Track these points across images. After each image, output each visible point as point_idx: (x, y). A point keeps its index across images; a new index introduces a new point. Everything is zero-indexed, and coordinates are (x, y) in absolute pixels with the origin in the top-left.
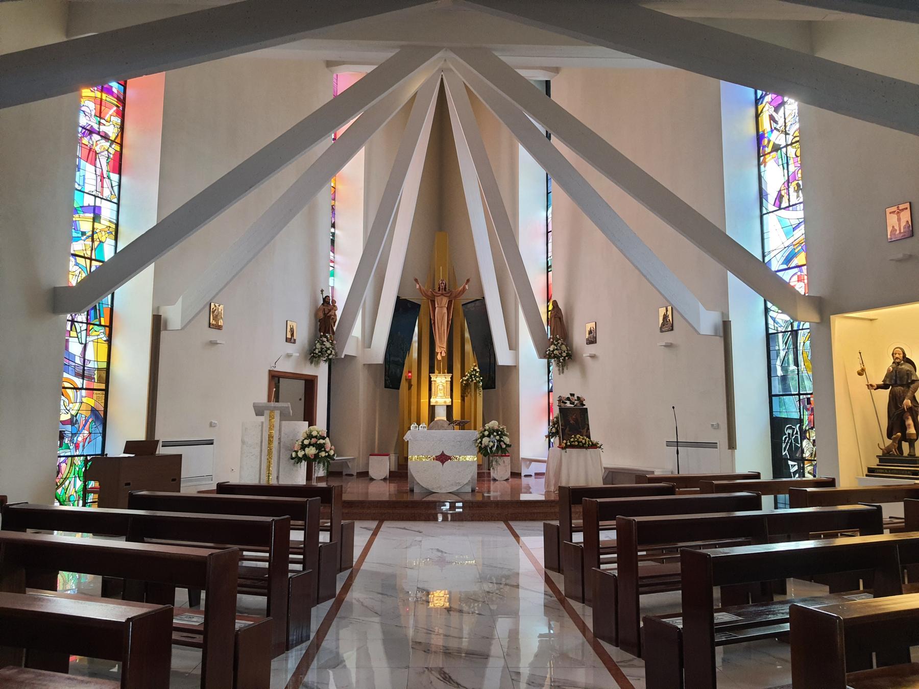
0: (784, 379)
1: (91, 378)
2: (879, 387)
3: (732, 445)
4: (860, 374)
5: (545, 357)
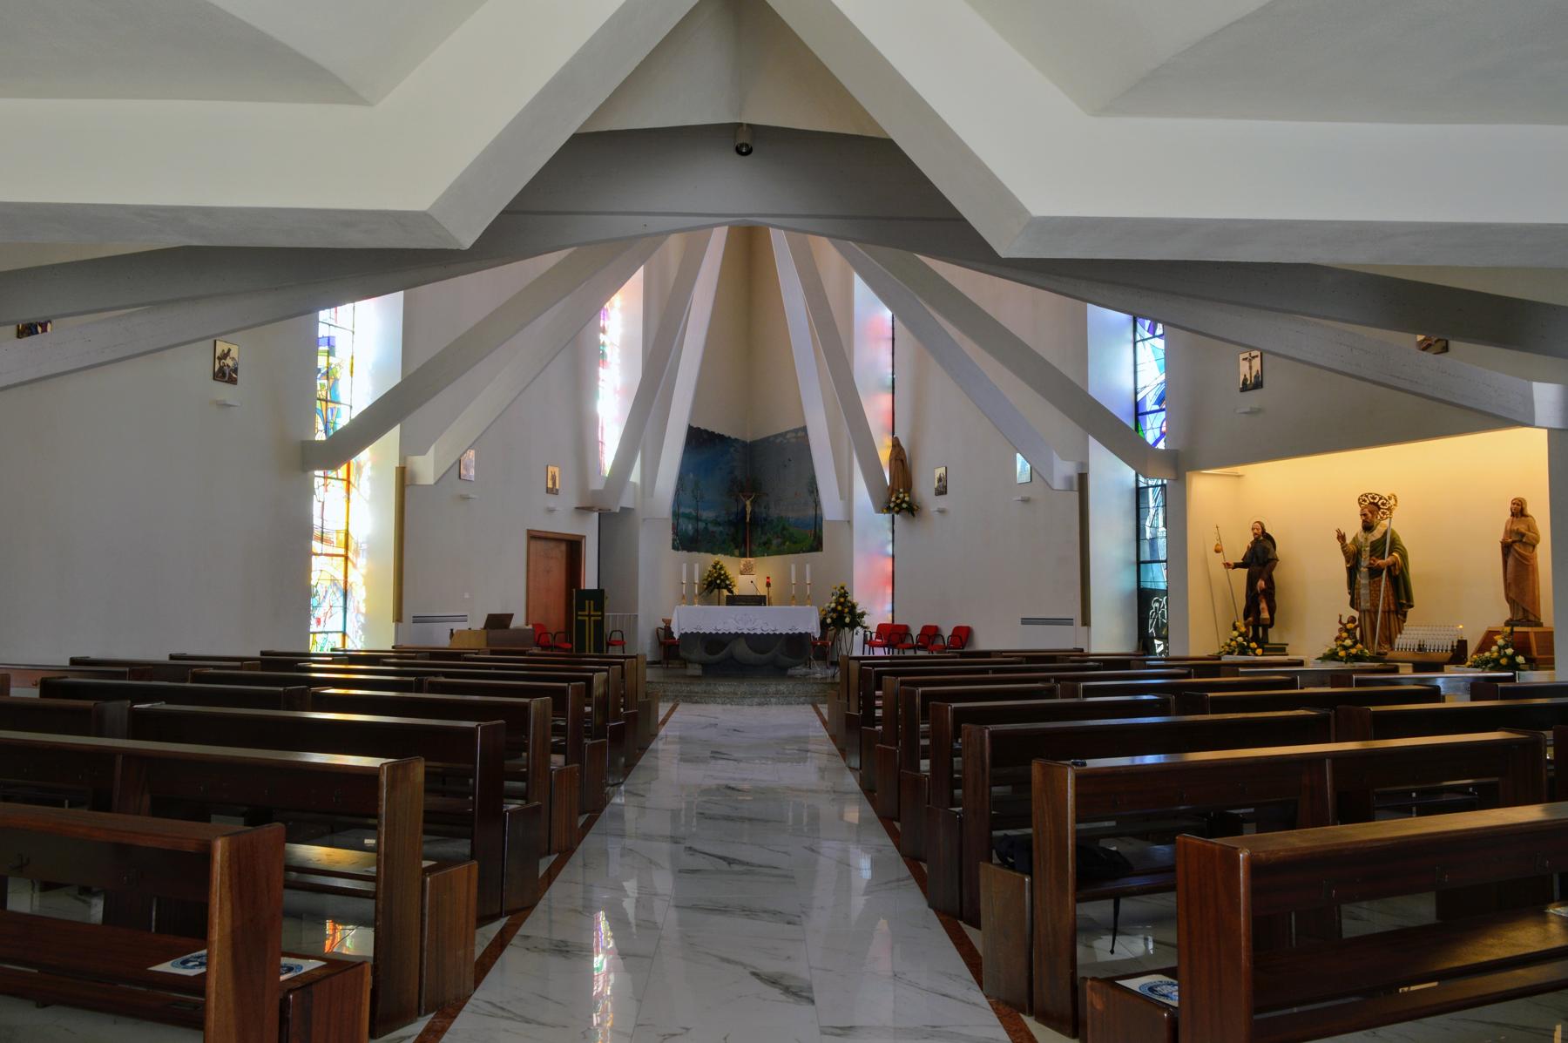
0: (1153, 540)
1: (330, 542)
2: (1237, 566)
3: (1086, 622)
4: (1217, 551)
5: (889, 509)
